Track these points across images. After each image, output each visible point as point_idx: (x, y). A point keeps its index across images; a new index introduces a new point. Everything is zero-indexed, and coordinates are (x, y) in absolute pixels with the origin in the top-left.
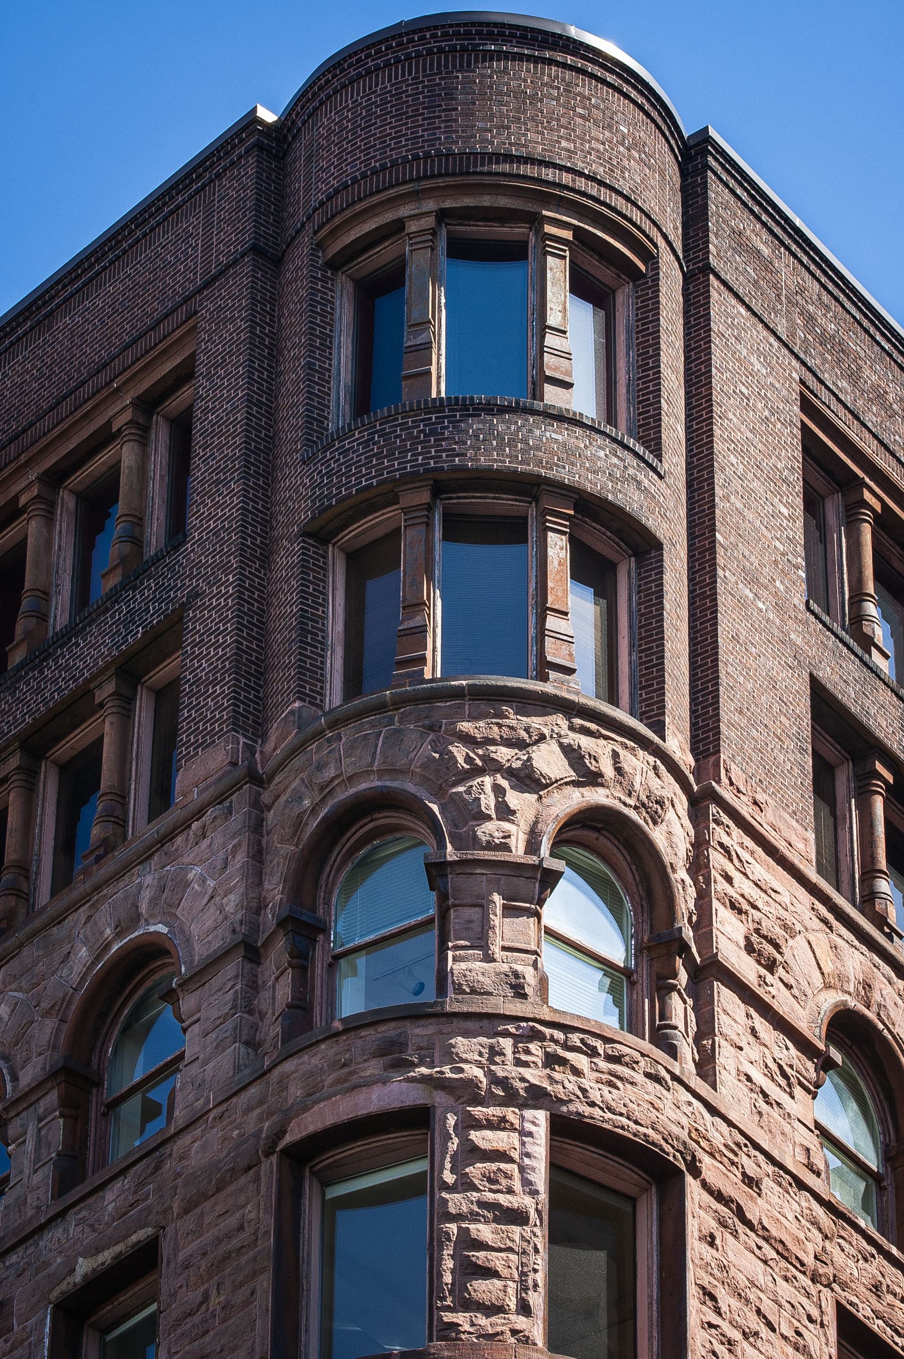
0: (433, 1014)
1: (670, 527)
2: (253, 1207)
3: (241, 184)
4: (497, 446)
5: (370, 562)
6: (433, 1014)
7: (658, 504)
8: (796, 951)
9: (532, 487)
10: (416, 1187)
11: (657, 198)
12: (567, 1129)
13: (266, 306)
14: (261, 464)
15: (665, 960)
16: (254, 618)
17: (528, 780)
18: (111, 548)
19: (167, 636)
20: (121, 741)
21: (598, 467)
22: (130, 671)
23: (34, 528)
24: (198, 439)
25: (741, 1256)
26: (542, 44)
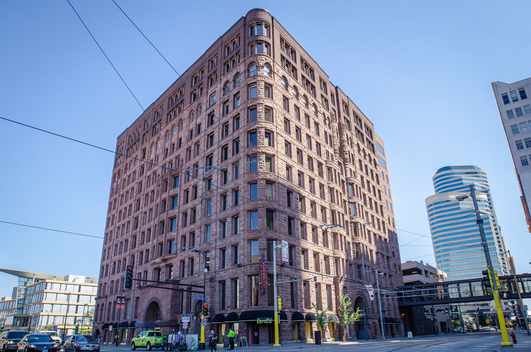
0: (256, 76)
1: (271, 43)
2: (246, 88)
3: (243, 21)
4: (260, 38)
5: (252, 46)
6: (256, 76)
7: (270, 42)
8: (280, 71)
9: (262, 41)
10: (256, 87)
11: (270, 21)
12: (265, 83)
13: (245, 29)
14: (245, 40)
15: (271, 72)
16: (245, 50)
17: (262, 60)
18: (235, 46)
19: (239, 52)
20: (236, 58)
21: (267, 39)
22: (237, 54)
23: (235, 58)
24: (197, 211)
25: (276, 91)
26: (262, 10)
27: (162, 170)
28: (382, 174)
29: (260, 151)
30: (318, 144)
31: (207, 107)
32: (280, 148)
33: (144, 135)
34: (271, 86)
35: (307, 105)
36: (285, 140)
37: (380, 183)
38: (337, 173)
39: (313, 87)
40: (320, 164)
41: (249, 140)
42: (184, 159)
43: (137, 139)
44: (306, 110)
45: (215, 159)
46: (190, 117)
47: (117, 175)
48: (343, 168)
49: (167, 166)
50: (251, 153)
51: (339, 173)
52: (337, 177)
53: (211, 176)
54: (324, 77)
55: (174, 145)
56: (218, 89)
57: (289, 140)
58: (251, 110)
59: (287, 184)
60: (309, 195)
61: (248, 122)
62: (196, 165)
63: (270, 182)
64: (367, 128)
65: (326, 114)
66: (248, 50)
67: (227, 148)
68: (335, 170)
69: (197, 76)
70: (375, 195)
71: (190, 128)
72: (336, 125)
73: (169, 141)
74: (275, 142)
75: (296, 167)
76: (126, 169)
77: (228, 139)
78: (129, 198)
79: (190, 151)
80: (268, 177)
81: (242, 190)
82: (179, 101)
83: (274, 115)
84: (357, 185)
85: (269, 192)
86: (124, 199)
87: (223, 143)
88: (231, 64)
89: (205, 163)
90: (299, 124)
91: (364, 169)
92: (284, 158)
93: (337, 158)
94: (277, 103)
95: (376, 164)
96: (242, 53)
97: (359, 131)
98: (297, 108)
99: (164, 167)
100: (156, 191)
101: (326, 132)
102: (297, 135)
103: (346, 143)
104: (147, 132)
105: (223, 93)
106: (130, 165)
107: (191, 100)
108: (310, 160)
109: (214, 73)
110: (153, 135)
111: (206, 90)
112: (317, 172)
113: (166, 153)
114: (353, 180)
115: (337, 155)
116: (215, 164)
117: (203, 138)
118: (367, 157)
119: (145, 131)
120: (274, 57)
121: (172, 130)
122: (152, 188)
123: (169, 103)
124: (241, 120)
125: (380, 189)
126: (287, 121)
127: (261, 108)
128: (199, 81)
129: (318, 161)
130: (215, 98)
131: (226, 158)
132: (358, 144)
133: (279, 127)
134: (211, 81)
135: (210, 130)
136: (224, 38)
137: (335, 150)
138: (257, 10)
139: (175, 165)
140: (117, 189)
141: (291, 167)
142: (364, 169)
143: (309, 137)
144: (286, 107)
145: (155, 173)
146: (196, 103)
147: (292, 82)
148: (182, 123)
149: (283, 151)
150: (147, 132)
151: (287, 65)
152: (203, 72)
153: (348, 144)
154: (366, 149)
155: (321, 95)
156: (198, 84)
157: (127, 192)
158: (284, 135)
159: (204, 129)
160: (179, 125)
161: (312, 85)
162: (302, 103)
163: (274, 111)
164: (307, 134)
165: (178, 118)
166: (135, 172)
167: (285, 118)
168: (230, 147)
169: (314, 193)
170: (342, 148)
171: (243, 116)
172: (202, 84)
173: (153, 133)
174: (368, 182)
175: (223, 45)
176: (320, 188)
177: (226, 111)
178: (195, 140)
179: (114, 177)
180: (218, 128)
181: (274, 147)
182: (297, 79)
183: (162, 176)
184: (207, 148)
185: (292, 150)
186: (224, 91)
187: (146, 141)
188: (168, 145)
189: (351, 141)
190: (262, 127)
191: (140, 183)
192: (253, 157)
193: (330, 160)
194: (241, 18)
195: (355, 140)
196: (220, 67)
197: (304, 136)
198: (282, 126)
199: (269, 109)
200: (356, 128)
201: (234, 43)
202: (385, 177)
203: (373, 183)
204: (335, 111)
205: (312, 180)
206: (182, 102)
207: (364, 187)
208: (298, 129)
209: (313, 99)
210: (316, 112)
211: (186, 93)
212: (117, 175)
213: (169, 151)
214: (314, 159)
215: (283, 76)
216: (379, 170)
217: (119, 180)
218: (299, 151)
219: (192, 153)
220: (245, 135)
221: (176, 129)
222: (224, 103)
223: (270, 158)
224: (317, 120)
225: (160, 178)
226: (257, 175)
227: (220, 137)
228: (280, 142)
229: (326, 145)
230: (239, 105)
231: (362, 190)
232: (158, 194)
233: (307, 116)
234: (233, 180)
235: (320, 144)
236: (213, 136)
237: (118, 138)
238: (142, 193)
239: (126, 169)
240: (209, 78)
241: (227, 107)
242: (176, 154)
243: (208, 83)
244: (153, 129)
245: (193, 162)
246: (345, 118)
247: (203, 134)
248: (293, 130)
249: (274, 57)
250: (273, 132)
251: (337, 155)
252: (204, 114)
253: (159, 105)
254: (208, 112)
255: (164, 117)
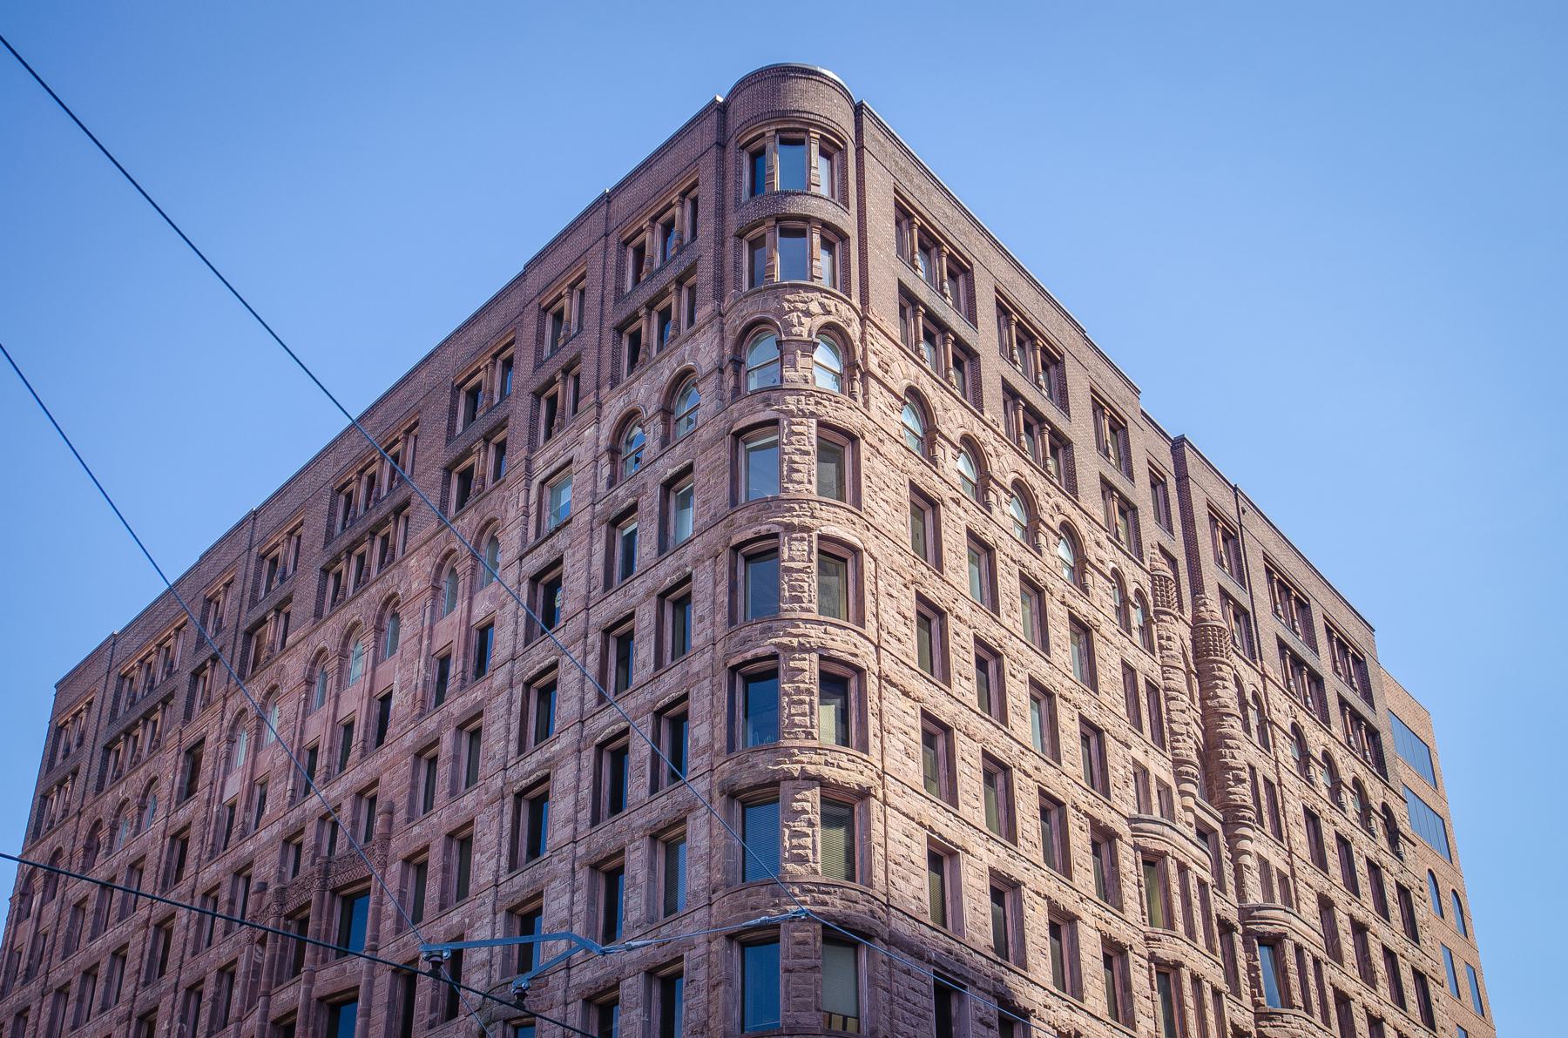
1: (852, 232)
4: (797, 206)
5: (756, 244)
8: (894, 367)
9: (807, 219)
10: (775, 444)
13: (721, 160)
14: (721, 213)
15: (853, 371)
16: (719, 264)
17: (808, 314)
18: (673, 241)
19: (691, 270)
20: (677, 303)
21: (830, 212)
22: (680, 282)
25: (878, 464)
26: (808, 73)
27: (283, 861)
28: (1428, 887)
29: (796, 769)
30: (1092, 733)
31: (524, 541)
32: (897, 752)
33: (196, 675)
34: (853, 438)
35: (1032, 530)
36: (926, 715)
37: (1423, 935)
38: (1193, 883)
39: (1061, 444)
40: (1104, 839)
41: (740, 714)
42: (401, 803)
43: (160, 694)
44: (1027, 558)
45: (560, 808)
46: (436, 588)
47: (39, 881)
48: (1225, 854)
49: (309, 839)
50: (746, 779)
51: (1202, 884)
52: (1196, 903)
53: (539, 895)
54: (1114, 391)
55: (349, 727)
56: (583, 453)
57: (945, 710)
58: (749, 558)
59: (935, 941)
60: (1051, 1001)
61: (732, 620)
62: (462, 840)
63: (843, 936)
64: (1342, 645)
65: (1128, 578)
66: (737, 266)
67: (624, 750)
68: (1183, 868)
69: (478, 387)
70: (1400, 1000)
71: (438, 644)
72: (1179, 632)
73: (327, 709)
74: (873, 722)
75: (981, 851)
76: (91, 848)
77: (631, 703)
78: (96, 1006)
79: (433, 761)
80: (836, 905)
81: (701, 976)
82: (385, 509)
83: (868, 586)
84: (1299, 949)
85: (840, 987)
86: (71, 1008)
87: (604, 724)
88: (649, 329)
89: (507, 825)
90: (996, 631)
91: (1333, 859)
92: (917, 805)
93: (1190, 802)
94: (880, 525)
95: (1393, 835)
96: (704, 276)
97: (1298, 662)
98: (981, 549)
99: (292, 841)
100: (241, 968)
101: (1129, 670)
102: (984, 684)
103: (1233, 727)
104: (215, 659)
105: (606, 471)
106: (114, 828)
107: (444, 504)
108: (1054, 816)
109: (566, 371)
110: (242, 675)
111: (523, 453)
112: (1091, 877)
113: (307, 761)
114: (1277, 919)
115: (1190, 788)
116: (557, 832)
117: (504, 697)
118: (1347, 797)
119: (206, 654)
120: (864, 299)
121: (343, 655)
122: (222, 952)
123: (332, 514)
124: (699, 608)
125: (1426, 966)
126: (930, 616)
127: (799, 548)
128: (491, 409)
129: (1095, 823)
130: (566, 496)
131: (617, 805)
132: (1294, 727)
133: (894, 646)
134: (552, 413)
135: (540, 656)
136: (620, 203)
137: (1178, 762)
138: (782, 73)
139: (354, 834)
140: (37, 956)
141: (953, 855)
142: (1333, 859)
143: (1042, 694)
144: (929, 548)
145: (242, 872)
146: (469, 522)
147: (954, 419)
148: (395, 616)
149: (914, 772)
150: (215, 659)
151: (929, 337)
152: (508, 364)
153: (1247, 728)
154: (1338, 753)
155: (1103, 480)
156: (483, 423)
157: (90, 973)
158: (919, 687)
159: (506, 653)
160: (379, 629)
161: (1056, 434)
162: (1007, 523)
163: (869, 566)
164: (1034, 683)
165: (375, 592)
166: (136, 867)
167: (921, 598)
168: (640, 749)
169: (1078, 992)
170: (1213, 747)
171: (709, 591)
172: (502, 425)
173: (243, 664)
174: (1359, 929)
175: (613, 239)
176: (1108, 962)
177: (621, 564)
178: (457, 706)
179: (24, 893)
180: (579, 647)
181: (864, 747)
182: (978, 403)
183: (281, 892)
184: (521, 749)
185: (960, 765)
186: (613, 461)
187: (208, 703)
188: (318, 729)
189: (1260, 712)
190: (803, 649)
191: (163, 928)
192: (756, 802)
193: (1156, 814)
194: (706, 110)
195: (1282, 709)
196: (594, 346)
197: (1018, 693)
198: (909, 641)
199: (838, 558)
200: (1282, 646)
201: (668, 228)
202: (1448, 902)
203: (1386, 934)
204: (1173, 562)
205: (1062, 923)
206: (398, 511)
207: (1336, 953)
208: (988, 658)
209: (1061, 500)
210: (1080, 566)
211: (419, 468)
212: (39, 881)
213: (322, 761)
214: (1071, 811)
215: (912, 391)
216: (1415, 865)
217: (52, 908)
218: (996, 771)
219: (443, 771)
220: (726, 675)
221: (364, 645)
222: (615, 523)
223: (845, 808)
224: (1082, 608)
225: (269, 896)
226: (775, 895)
227: (591, 696)
228: (896, 722)
229: (1133, 739)
230: (689, 531)
231: (1329, 972)
232: (255, 985)
233: (1033, 589)
234: (651, 920)
235: (1098, 732)
236: (553, 686)
237: (63, 686)
238: (168, 980)
239: (91, 848)
240: (537, 395)
241: (630, 540)
242: (355, 776)
243: (534, 419)
244: (247, 642)
245: (443, 818)
246: (1225, 595)
247: (500, 678)
248: (963, 661)
249: (864, 299)
250: (860, 671)
251: (1190, 788)
252: (511, 577)
253: (283, 522)
254: (534, 563)
255: (306, 587)
